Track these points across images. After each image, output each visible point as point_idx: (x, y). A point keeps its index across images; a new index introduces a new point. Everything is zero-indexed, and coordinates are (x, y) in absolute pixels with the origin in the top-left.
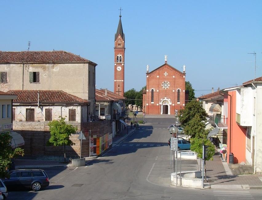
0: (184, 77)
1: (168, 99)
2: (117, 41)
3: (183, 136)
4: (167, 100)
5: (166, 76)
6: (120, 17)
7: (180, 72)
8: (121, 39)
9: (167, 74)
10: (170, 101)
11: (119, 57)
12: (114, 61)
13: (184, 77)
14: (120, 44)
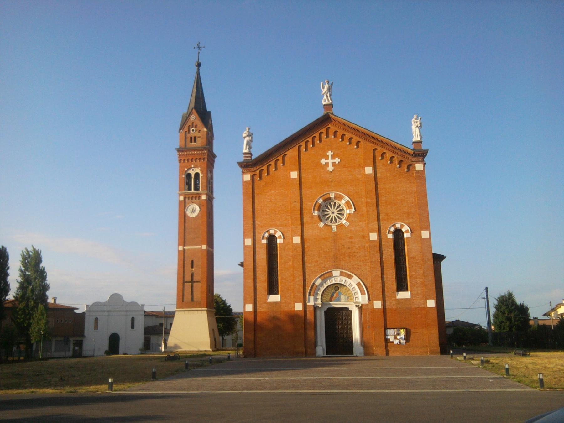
0: (419, 167)
1: (350, 277)
2: (186, 129)
3: (300, 143)
4: (343, 280)
5: (330, 168)
6: (199, 65)
7: (396, 149)
8: (199, 123)
9: (337, 160)
10: (344, 279)
11: (193, 176)
12: (177, 188)
13: (419, 167)
14: (195, 138)
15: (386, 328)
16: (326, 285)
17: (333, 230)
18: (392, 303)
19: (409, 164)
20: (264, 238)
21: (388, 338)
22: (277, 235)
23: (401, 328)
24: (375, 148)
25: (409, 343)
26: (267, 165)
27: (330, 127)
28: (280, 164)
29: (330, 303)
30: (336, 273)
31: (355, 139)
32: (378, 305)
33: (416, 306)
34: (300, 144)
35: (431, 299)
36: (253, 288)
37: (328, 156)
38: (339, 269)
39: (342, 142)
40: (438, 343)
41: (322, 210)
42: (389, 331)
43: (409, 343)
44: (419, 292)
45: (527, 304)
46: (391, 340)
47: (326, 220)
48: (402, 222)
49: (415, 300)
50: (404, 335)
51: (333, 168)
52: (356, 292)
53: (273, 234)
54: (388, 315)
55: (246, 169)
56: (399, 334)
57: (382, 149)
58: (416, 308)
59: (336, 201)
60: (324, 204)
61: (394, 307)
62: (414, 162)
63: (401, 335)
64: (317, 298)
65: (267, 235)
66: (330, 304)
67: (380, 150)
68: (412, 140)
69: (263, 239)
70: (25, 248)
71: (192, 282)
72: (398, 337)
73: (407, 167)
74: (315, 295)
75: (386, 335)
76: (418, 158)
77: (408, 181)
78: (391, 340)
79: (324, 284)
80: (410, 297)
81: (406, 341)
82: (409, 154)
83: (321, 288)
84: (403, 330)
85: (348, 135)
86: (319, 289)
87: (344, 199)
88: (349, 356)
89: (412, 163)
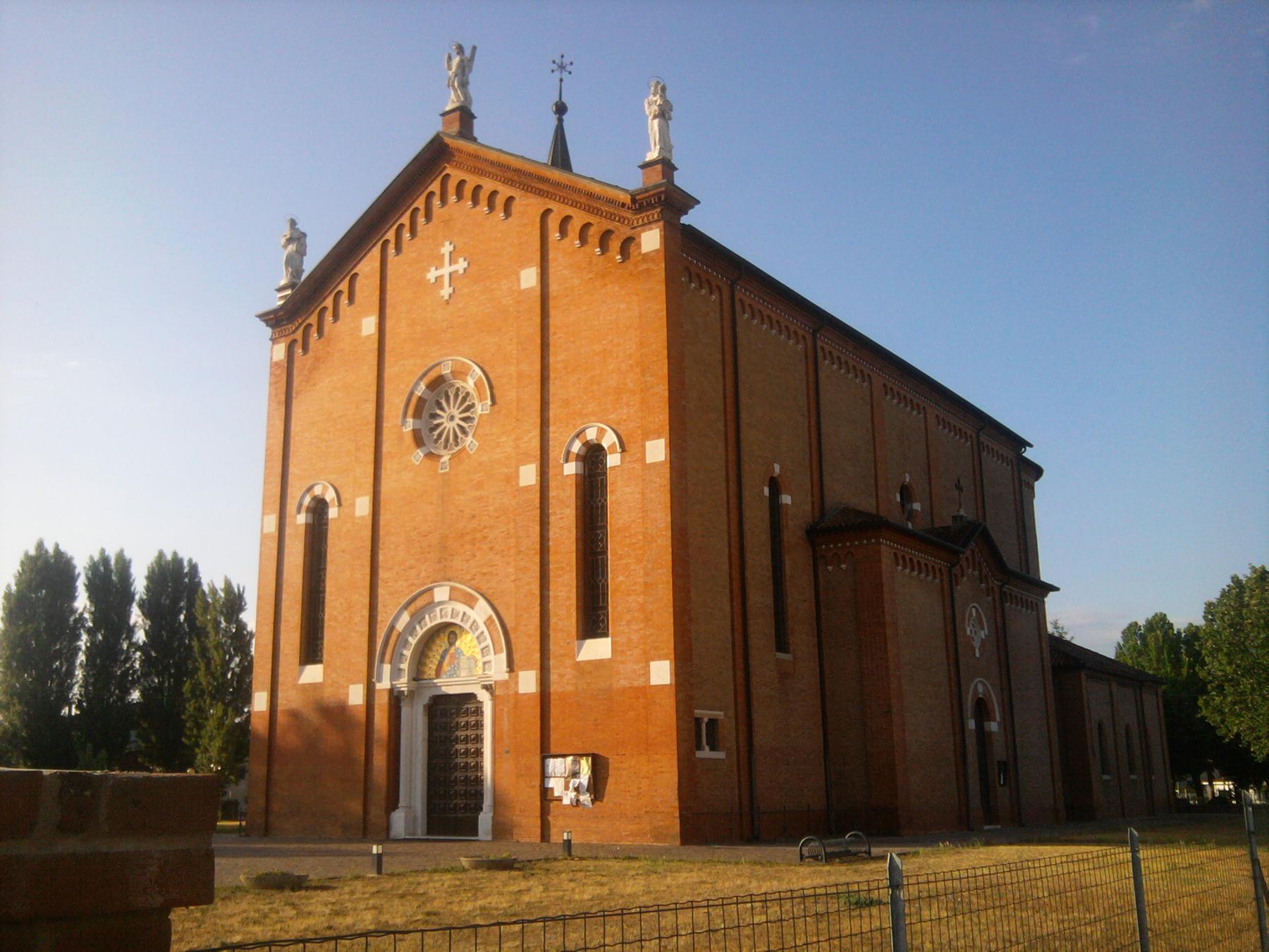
1: (470, 602)
15: (546, 753)
16: (422, 629)
17: (442, 469)
18: (564, 675)
19: (625, 237)
20: (571, 455)
21: (550, 786)
22: (605, 444)
23: (581, 755)
24: (545, 209)
25: (602, 801)
26: (318, 310)
27: (449, 172)
28: (344, 300)
29: (435, 681)
30: (441, 593)
31: (505, 191)
32: (528, 682)
33: (624, 683)
34: (398, 223)
35: (660, 658)
36: (270, 647)
37: (443, 255)
38: (449, 580)
39: (474, 210)
40: (676, 804)
41: (428, 415)
42: (557, 766)
43: (602, 801)
44: (635, 637)
45: (212, 581)
46: (556, 794)
47: (436, 441)
48: (601, 422)
49: (622, 662)
50: (587, 777)
51: (451, 290)
52: (486, 647)
53: (596, 442)
54: (554, 712)
55: (279, 329)
56: (575, 774)
57: (563, 206)
58: (624, 691)
59: (459, 383)
60: (430, 397)
61: (570, 688)
62: (639, 229)
63: (582, 775)
64: (400, 670)
65: (577, 447)
66: (435, 686)
67: (559, 210)
68: (645, 157)
69: (567, 461)
70: (99, 549)
71: (723, 905)
72: (574, 782)
73: (619, 250)
74: (396, 659)
75: (544, 776)
76: (649, 213)
77: (623, 292)
78: (556, 794)
79: (418, 627)
80: (609, 656)
81: (592, 796)
82: (623, 205)
83: (410, 639)
84: (587, 761)
85: (488, 185)
86: (406, 642)
87: (471, 376)
88: (455, 841)
89: (633, 231)
